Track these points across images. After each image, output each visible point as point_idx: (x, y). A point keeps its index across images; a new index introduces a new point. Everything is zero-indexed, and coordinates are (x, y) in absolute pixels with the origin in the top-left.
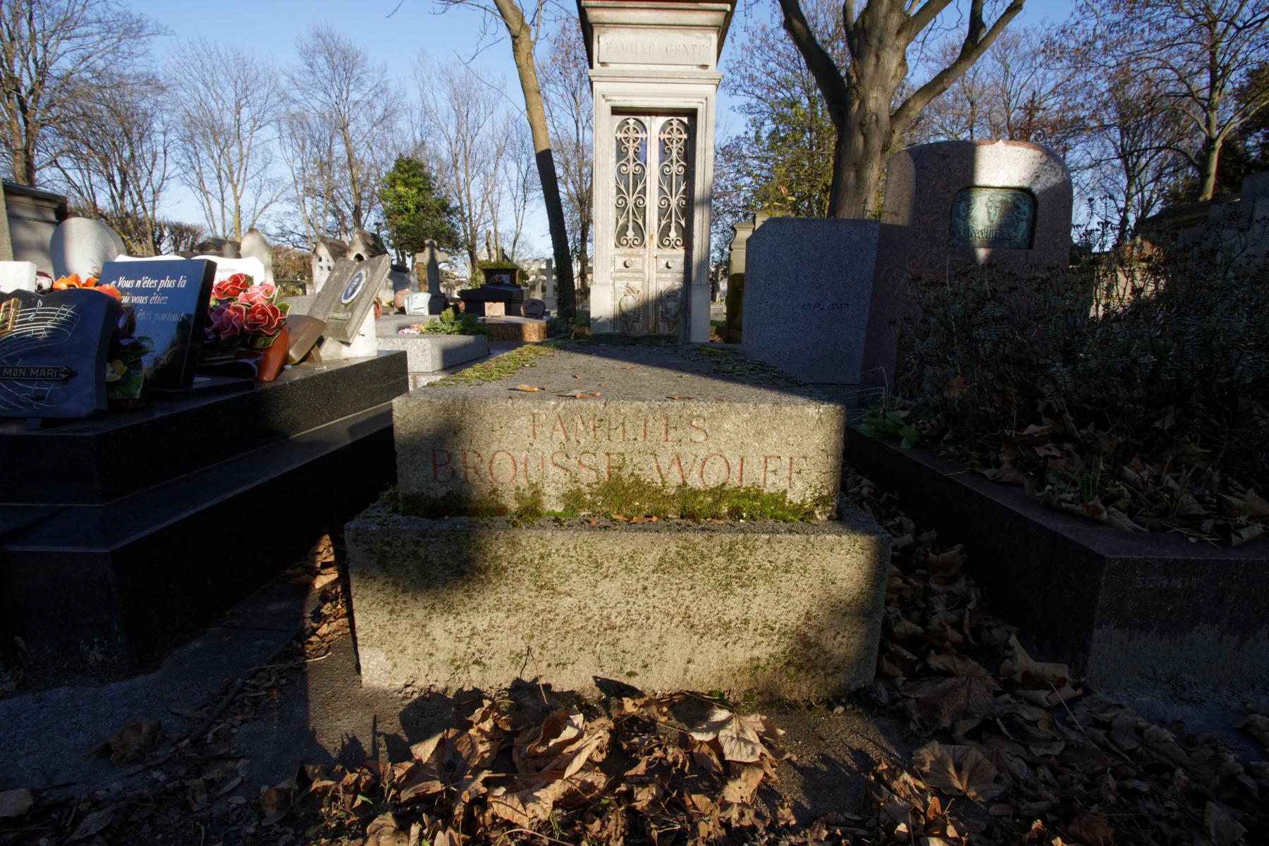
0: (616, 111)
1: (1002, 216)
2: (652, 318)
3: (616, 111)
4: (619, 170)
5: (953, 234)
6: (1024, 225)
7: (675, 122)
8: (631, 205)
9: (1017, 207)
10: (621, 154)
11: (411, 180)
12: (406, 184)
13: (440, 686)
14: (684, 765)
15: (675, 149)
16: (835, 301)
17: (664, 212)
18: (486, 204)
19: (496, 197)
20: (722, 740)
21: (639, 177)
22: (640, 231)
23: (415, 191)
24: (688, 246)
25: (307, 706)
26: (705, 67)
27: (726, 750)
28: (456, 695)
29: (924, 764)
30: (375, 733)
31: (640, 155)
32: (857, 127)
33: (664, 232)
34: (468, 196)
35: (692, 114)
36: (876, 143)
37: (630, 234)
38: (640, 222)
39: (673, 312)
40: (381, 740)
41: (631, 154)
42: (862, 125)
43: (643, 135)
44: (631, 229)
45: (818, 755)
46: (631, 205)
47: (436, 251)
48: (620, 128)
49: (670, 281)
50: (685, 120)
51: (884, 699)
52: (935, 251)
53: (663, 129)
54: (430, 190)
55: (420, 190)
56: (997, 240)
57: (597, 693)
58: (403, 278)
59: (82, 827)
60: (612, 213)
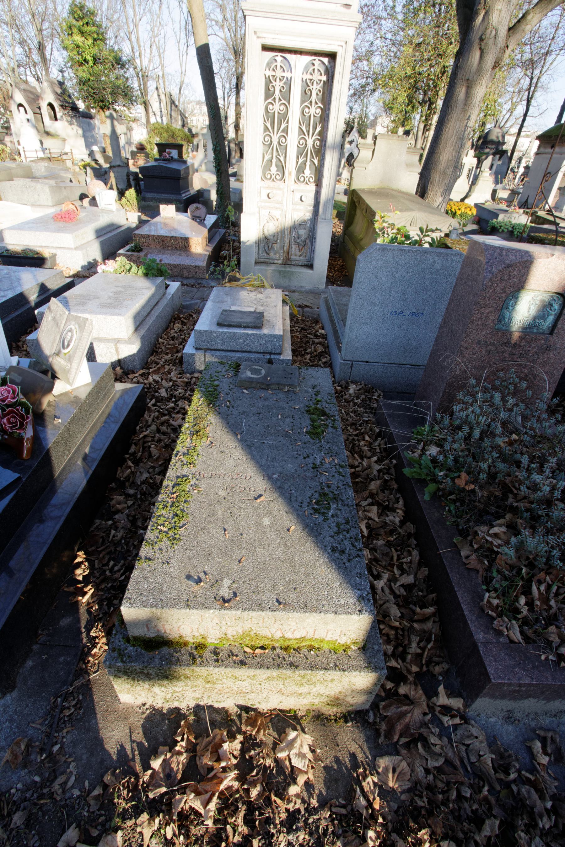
0: (266, 48)
1: (539, 311)
2: (287, 241)
3: (266, 48)
4: (266, 108)
5: (500, 321)
6: (551, 318)
7: (317, 63)
8: (275, 142)
9: (551, 305)
10: (269, 94)
11: (86, 29)
12: (82, 33)
13: (160, 705)
14: (273, 768)
15: (316, 89)
16: (414, 310)
17: (301, 152)
18: (154, 47)
19: (162, 41)
20: (291, 756)
21: (284, 116)
22: (282, 168)
23: (90, 41)
24: (318, 184)
25: (96, 718)
26: (348, 6)
27: (293, 761)
28: (167, 711)
29: (379, 768)
30: (133, 741)
31: (286, 96)
32: (477, 41)
33: (301, 170)
34: (138, 39)
35: (332, 56)
36: (490, 60)
37: (274, 169)
38: (282, 159)
39: (303, 238)
40: (135, 745)
41: (277, 93)
42: (481, 39)
43: (287, 75)
44: (275, 166)
45: (334, 757)
46: (275, 142)
47: (116, 123)
48: (269, 65)
49: (303, 212)
50: (326, 60)
51: (371, 720)
52: (484, 333)
53: (306, 70)
54: (104, 40)
55: (95, 40)
56: (529, 330)
57: (236, 709)
58: (89, 124)
59: (13, 822)
60: (260, 149)
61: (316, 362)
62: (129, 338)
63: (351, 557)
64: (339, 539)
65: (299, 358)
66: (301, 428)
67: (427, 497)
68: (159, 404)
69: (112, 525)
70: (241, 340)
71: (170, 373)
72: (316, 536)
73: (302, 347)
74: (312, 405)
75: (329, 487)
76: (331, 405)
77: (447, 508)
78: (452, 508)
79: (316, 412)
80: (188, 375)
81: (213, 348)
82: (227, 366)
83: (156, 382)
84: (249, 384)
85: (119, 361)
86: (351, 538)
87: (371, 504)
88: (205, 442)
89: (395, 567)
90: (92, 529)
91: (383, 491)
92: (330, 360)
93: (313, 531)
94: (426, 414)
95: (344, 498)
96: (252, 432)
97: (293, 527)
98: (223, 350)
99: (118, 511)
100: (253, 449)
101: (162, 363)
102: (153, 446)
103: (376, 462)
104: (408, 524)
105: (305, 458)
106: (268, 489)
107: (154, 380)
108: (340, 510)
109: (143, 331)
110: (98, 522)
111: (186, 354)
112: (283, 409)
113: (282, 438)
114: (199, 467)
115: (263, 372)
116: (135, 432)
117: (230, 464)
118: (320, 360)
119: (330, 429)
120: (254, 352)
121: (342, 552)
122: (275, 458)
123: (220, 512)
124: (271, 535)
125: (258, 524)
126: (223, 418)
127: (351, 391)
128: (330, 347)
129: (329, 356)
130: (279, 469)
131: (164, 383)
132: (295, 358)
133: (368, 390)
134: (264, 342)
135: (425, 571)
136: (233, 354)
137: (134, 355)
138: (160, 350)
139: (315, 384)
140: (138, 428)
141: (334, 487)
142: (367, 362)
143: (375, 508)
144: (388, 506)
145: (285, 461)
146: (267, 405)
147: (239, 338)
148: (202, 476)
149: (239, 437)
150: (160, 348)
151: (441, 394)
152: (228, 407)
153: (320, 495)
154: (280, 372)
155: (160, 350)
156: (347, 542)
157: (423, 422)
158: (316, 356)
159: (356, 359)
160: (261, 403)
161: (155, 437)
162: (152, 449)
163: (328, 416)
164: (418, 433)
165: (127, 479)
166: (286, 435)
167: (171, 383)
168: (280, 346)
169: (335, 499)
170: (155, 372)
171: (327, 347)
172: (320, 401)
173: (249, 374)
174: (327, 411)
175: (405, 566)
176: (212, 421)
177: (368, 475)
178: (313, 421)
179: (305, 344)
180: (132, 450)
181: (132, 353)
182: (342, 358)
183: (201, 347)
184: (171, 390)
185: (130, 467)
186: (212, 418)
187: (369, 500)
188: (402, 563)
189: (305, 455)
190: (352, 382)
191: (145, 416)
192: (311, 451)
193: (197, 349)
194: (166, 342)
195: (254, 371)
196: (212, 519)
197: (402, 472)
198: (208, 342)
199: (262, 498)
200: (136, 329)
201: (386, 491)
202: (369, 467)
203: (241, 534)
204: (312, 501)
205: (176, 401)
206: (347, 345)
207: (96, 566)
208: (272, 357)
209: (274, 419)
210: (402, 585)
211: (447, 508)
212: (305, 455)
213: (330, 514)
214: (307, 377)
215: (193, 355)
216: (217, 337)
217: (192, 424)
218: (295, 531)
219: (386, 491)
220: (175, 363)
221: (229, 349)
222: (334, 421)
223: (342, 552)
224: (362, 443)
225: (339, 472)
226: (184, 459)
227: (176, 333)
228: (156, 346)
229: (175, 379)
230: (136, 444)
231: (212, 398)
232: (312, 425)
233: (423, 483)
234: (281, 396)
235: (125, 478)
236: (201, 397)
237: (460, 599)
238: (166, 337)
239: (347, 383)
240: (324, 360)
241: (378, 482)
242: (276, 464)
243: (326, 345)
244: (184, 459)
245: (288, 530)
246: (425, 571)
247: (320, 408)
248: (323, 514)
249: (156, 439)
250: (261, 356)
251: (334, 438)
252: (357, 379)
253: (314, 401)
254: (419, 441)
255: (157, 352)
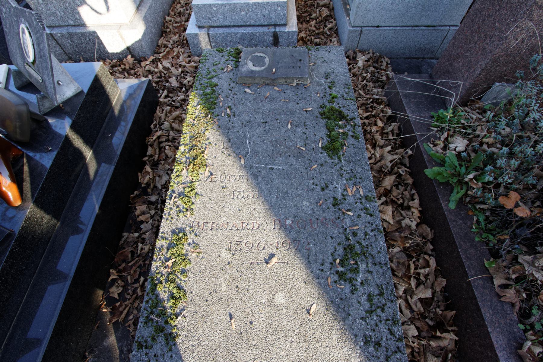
61: (322, 30)
62: (131, 22)
63: (390, 353)
64: (373, 322)
65: (305, 25)
66: (315, 142)
67: (452, 206)
68: (171, 95)
69: (138, 237)
70: (243, 13)
71: (178, 57)
72: (344, 320)
73: (306, 11)
74: (326, 103)
75: (355, 234)
76: (348, 102)
77: (475, 218)
78: (481, 219)
79: (332, 115)
80: (196, 58)
81: (215, 25)
82: (225, 54)
83: (167, 69)
84: (249, 80)
85: (128, 48)
86: (387, 320)
87: (385, 203)
88: (204, 173)
89: (412, 279)
90: (121, 242)
91: (397, 187)
92: (336, 25)
93: (340, 308)
94: (451, 95)
95: (374, 253)
96: (258, 153)
97: (314, 307)
98: (226, 27)
99: (142, 222)
100: (260, 179)
101: (170, 46)
102: (167, 147)
103: (389, 152)
104: (424, 226)
105: (323, 189)
106: (280, 246)
107: (164, 68)
108: (371, 272)
109: (144, 10)
110: (126, 234)
111: (189, 34)
112: (293, 113)
113: (293, 159)
114: (198, 215)
115: (267, 60)
116: (150, 132)
117: (233, 206)
118: (326, 26)
119: (350, 141)
120: (258, 26)
121: (378, 344)
122: (286, 193)
123: (224, 288)
124: (288, 323)
125: (271, 304)
126: (223, 133)
127: (360, 64)
128: (336, 10)
129: (335, 20)
130: (293, 210)
131: (173, 70)
132: (300, 26)
133: (375, 61)
134: (267, 12)
135: (443, 282)
136: (237, 30)
137: (140, 40)
138: (168, 30)
139: (329, 71)
140: (152, 126)
141: (361, 233)
142: (378, 27)
143: (389, 209)
144: (402, 204)
145: (298, 195)
146: (274, 110)
147: (241, 11)
148: (201, 227)
149: (243, 162)
150: (168, 28)
151: (477, 72)
152: (229, 116)
153: (345, 249)
154: (287, 60)
155: (168, 30)
156: (382, 327)
157: (444, 105)
158: (322, 21)
159: (366, 24)
160: (266, 107)
161: (168, 136)
162: (166, 151)
163: (347, 120)
164: (441, 119)
165: (148, 184)
166: (299, 155)
167: (180, 70)
168: (284, 15)
169: (364, 254)
170: (165, 57)
171: (332, 10)
172: (336, 97)
173: (250, 66)
174: (345, 111)
175: (422, 278)
176: (211, 140)
177: (381, 167)
178: (330, 129)
179: (310, 7)
180: (150, 151)
181: (137, 39)
182: (350, 23)
183: (204, 24)
184: (181, 78)
185: (148, 173)
186: (212, 135)
187: (383, 199)
188: (419, 274)
189: (323, 185)
190: (360, 51)
191: (158, 112)
192: (330, 178)
193: (200, 27)
194: (173, 19)
195: (258, 61)
196: (215, 299)
197: (424, 173)
198: (209, 18)
199: (274, 260)
200: (138, 8)
201: (400, 186)
202: (382, 157)
203: (251, 323)
204: (335, 260)
205: (187, 90)
206: (358, 7)
207: (129, 281)
208: (278, 29)
209: (283, 130)
210: (421, 300)
211: (475, 218)
212: (323, 185)
213: (359, 280)
214: (319, 62)
215: (196, 35)
216: (217, 11)
217: (187, 147)
218: (317, 312)
219: (400, 186)
220: (183, 44)
221: (232, 24)
222: (354, 126)
223: (378, 344)
224: (374, 129)
225: (366, 209)
226: (180, 202)
227: (183, 7)
228: (164, 26)
229: (183, 63)
230: (152, 146)
231: (210, 104)
232: (329, 136)
233: (448, 187)
234: (290, 93)
235: (147, 184)
236: (198, 104)
237: (495, 343)
238: (173, 13)
239: (355, 53)
240: (330, 26)
241: (393, 177)
242: (289, 203)
243: (331, 7)
244: (180, 202)
245: (308, 311)
246: (442, 281)
247: (337, 108)
248: (351, 280)
249: (170, 137)
250: (265, 29)
251: (355, 154)
252: (365, 47)
253: (329, 98)
254: (442, 130)
255: (166, 32)
